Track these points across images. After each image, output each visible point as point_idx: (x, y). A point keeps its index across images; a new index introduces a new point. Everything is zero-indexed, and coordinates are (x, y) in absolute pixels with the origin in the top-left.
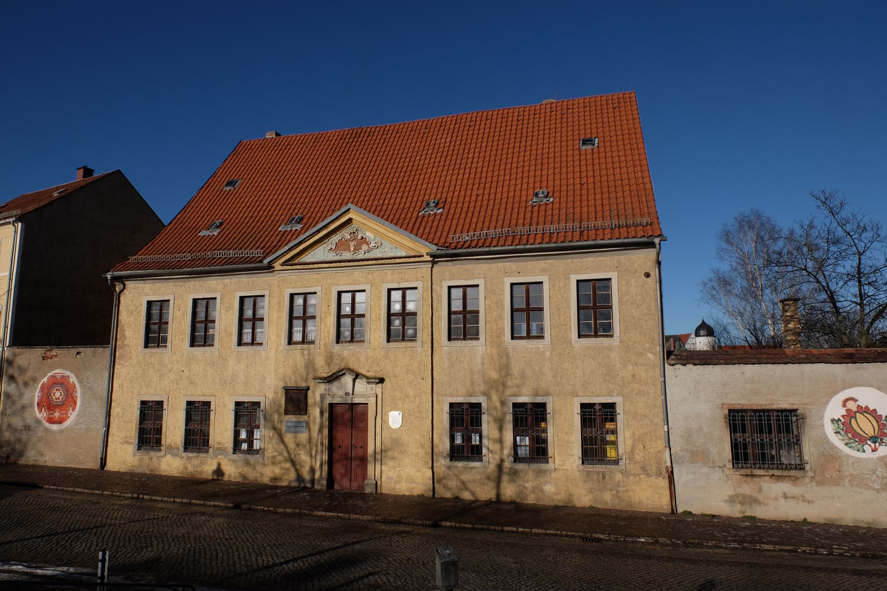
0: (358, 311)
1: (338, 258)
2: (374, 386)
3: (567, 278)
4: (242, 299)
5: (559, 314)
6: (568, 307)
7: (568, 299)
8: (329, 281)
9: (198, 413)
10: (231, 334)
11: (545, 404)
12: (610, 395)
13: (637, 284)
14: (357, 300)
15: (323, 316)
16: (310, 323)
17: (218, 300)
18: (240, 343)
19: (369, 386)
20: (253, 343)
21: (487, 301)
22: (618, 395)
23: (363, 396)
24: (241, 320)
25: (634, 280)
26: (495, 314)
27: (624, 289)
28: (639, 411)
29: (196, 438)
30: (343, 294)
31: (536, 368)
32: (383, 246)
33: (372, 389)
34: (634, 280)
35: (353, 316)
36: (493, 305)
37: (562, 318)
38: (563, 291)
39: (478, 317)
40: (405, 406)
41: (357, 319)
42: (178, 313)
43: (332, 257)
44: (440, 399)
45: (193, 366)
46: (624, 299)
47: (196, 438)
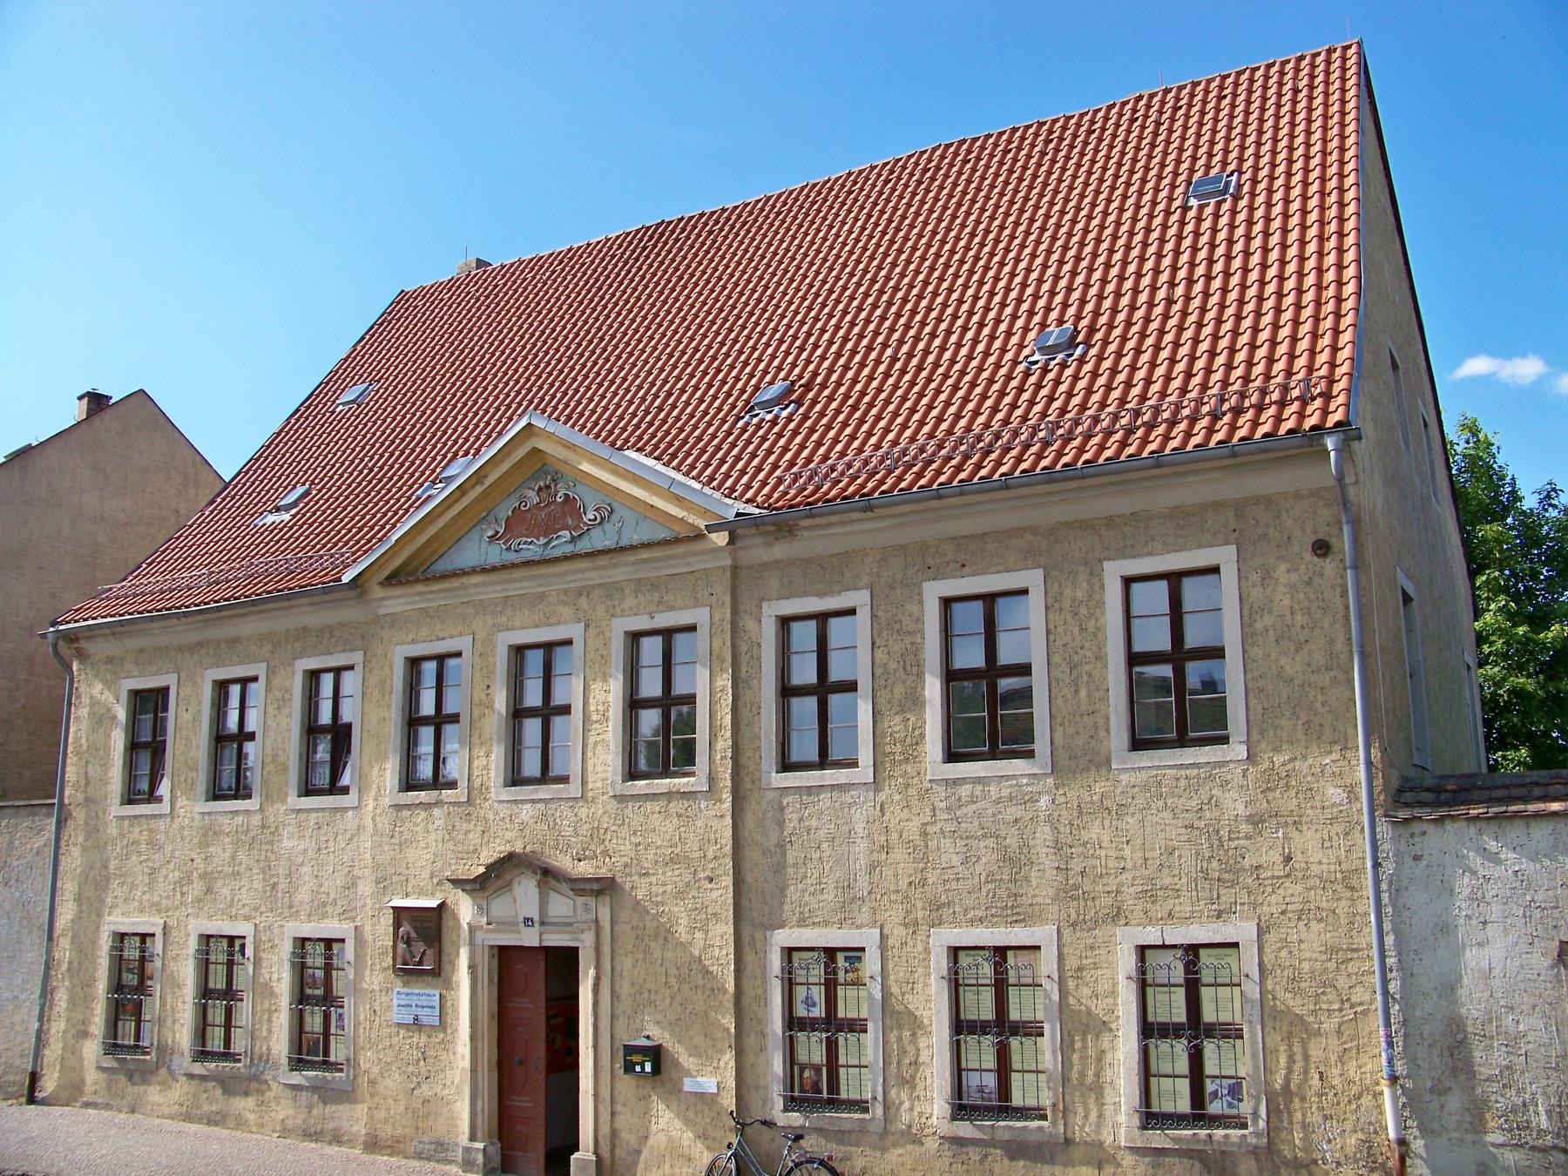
0: (449, 709)
1: (511, 557)
2: (591, 901)
3: (1096, 574)
4: (414, 663)
5: (1075, 681)
6: (1101, 657)
7: (1098, 634)
8: (490, 621)
10: (285, 768)
11: (576, 949)
13: (1294, 577)
14: (834, 641)
15: (476, 713)
16: (449, 729)
17: (578, 647)
18: (515, 778)
19: (580, 900)
20: (545, 777)
21: (879, 654)
23: (566, 925)
24: (413, 722)
25: (1283, 567)
26: (899, 690)
27: (1256, 594)
28: (1306, 966)
30: (956, 607)
31: (1012, 841)
32: (615, 517)
33: (587, 909)
34: (1283, 567)
35: (824, 688)
36: (893, 666)
37: (1083, 693)
38: (1083, 611)
39: (692, 715)
40: (669, 955)
42: (186, 717)
43: (495, 554)
44: (758, 936)
46: (1259, 626)
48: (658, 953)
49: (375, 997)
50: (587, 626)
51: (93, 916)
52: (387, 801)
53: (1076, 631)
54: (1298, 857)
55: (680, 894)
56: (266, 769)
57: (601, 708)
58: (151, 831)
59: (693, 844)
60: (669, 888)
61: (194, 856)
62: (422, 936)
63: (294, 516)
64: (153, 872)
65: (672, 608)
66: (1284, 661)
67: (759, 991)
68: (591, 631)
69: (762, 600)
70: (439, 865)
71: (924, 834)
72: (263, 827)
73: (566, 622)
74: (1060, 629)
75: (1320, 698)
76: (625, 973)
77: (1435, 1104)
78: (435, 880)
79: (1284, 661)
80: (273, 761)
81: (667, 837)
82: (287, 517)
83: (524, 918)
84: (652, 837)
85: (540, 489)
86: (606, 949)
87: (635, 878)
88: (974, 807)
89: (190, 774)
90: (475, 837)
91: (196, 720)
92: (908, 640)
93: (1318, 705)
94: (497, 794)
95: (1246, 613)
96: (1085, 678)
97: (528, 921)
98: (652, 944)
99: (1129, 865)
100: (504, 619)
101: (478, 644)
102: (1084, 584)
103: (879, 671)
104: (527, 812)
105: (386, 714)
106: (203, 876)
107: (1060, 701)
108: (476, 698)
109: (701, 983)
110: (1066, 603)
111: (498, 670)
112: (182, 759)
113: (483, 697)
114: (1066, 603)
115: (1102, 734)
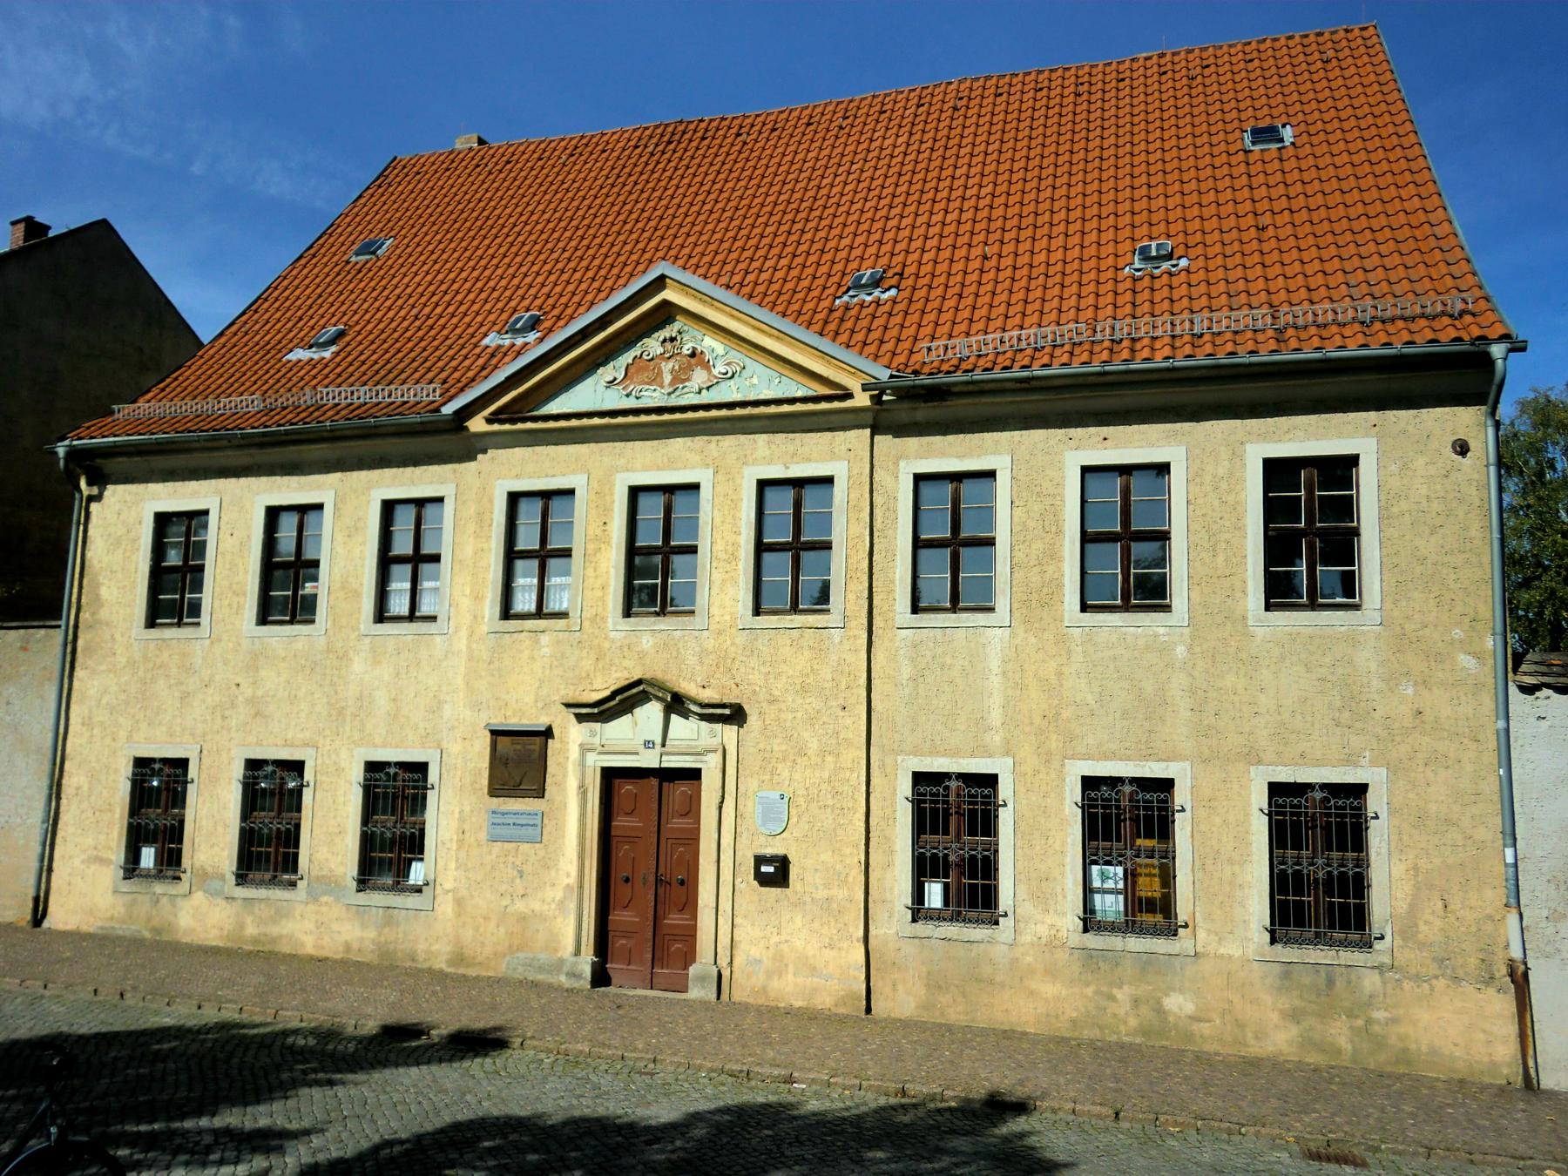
9: (273, 792)
12: (1350, 761)
13: (1432, 470)
15: (591, 547)
21: (1018, 512)
22: (1373, 763)
26: (1038, 546)
29: (269, 849)
31: (1149, 686)
36: (1031, 524)
38: (1224, 485)
41: (965, 553)
44: (888, 761)
45: (263, 673)
47: (269, 849)
48: (786, 774)
49: (453, 812)
50: (716, 472)
51: (108, 740)
52: (485, 629)
53: (1216, 503)
54: (1427, 711)
55: (811, 720)
56: (332, 597)
57: (730, 549)
58: (184, 655)
59: (826, 673)
60: (799, 715)
61: (238, 680)
62: (518, 761)
63: (337, 354)
64: (185, 697)
65: (809, 460)
66: (1417, 542)
67: (889, 811)
68: (720, 477)
69: (899, 458)
70: (544, 691)
71: (1060, 674)
72: (329, 651)
73: (693, 467)
74: (1200, 501)
75: (1453, 577)
76: (750, 793)
77: (1551, 930)
78: (540, 705)
79: (1417, 542)
80: (343, 588)
81: (799, 668)
82: (327, 354)
83: (637, 738)
84: (783, 667)
85: (665, 341)
86: (731, 770)
87: (764, 704)
88: (1111, 653)
89: (236, 599)
90: (587, 664)
91: (244, 544)
92: (1048, 501)
93: (1451, 582)
94: (615, 624)
95: (1383, 498)
96: (1223, 545)
97: (648, 744)
98: (780, 766)
99: (1263, 710)
100: (623, 461)
101: (594, 484)
102: (1226, 463)
103: (1017, 529)
104: (647, 642)
105: (485, 546)
106: (251, 701)
107: (1198, 564)
108: (591, 532)
109: (830, 802)
110: (1208, 478)
111: (616, 509)
112: (226, 583)
113: (599, 532)
114: (1208, 478)
115: (1238, 594)
